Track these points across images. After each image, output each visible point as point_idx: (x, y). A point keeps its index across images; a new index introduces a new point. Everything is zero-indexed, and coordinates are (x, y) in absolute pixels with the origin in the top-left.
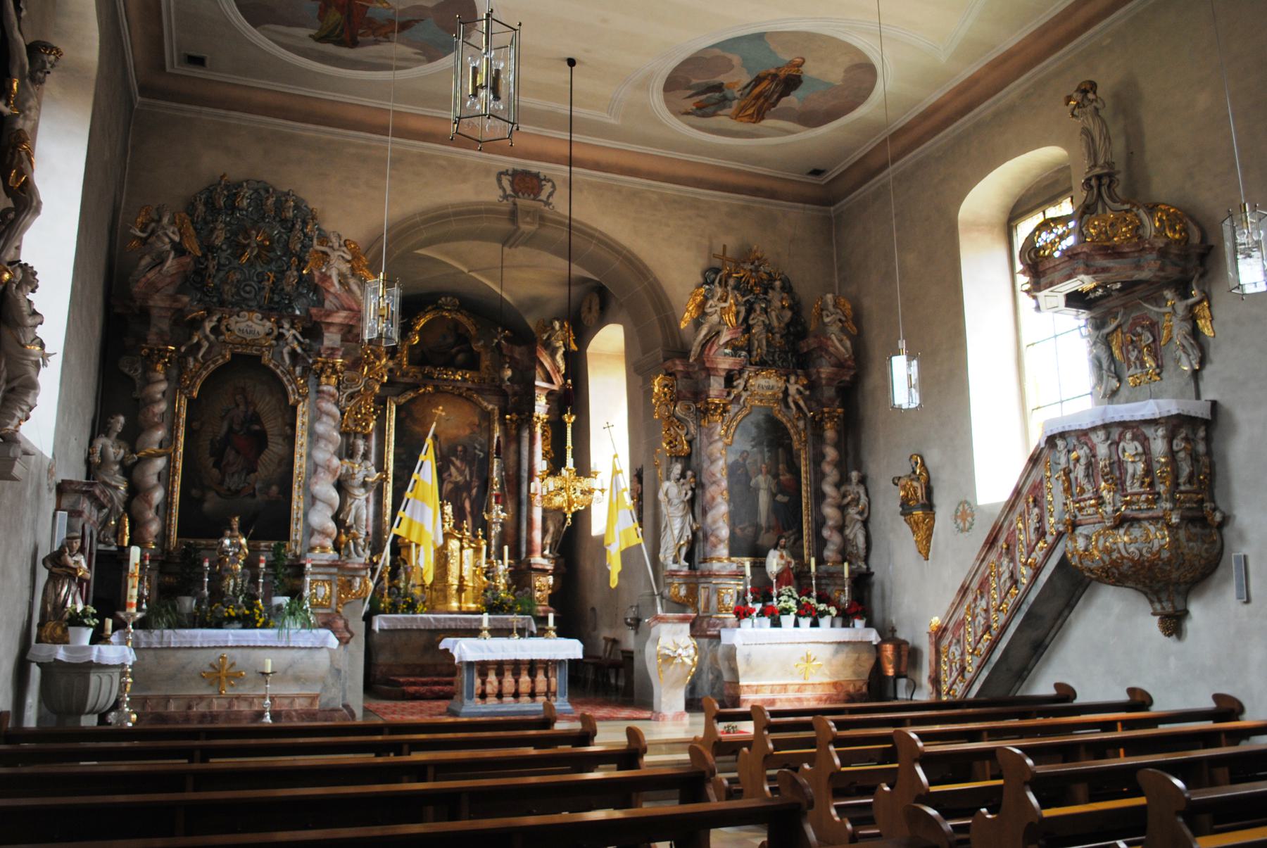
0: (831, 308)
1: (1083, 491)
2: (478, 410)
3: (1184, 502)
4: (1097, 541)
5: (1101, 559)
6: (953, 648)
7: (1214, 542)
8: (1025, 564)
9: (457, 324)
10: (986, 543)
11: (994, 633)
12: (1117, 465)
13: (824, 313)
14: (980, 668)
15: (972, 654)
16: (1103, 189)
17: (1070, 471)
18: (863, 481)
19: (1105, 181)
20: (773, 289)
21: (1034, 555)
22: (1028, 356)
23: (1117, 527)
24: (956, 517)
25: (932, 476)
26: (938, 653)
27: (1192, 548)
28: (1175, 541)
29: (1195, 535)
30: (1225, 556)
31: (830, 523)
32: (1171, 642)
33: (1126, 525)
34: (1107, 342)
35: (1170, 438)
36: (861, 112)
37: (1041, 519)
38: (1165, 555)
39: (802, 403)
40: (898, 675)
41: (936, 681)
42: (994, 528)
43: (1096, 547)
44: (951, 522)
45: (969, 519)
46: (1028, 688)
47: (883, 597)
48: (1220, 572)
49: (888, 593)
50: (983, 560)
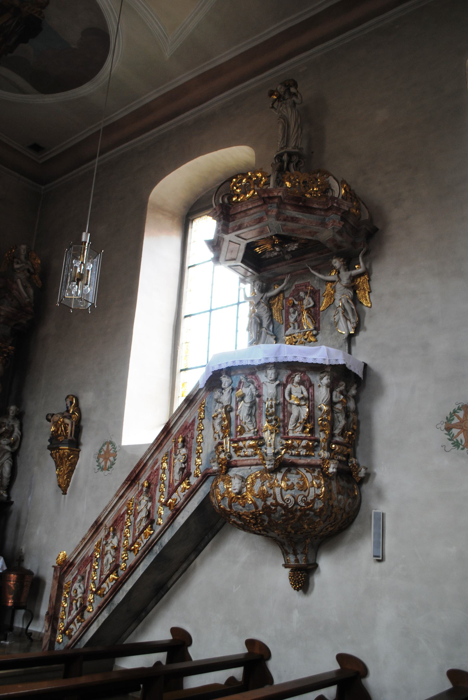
0: (23, 257)
3: (337, 453)
4: (253, 483)
5: (254, 504)
6: (76, 585)
7: (355, 497)
8: (164, 505)
10: (127, 480)
11: (121, 573)
12: (282, 406)
13: (15, 260)
14: (101, 609)
15: (95, 593)
16: (292, 166)
18: (20, 416)
19: (295, 158)
21: (175, 496)
22: (185, 324)
23: (274, 471)
25: (84, 416)
26: (60, 588)
27: (339, 502)
28: (329, 491)
29: (343, 487)
30: (361, 513)
32: (297, 597)
33: (284, 470)
34: (269, 303)
35: (331, 387)
37: (187, 460)
38: (319, 505)
40: (17, 606)
41: (53, 618)
42: (138, 465)
44: (93, 462)
45: (112, 459)
46: (144, 630)
47: (18, 526)
48: (355, 528)
49: (22, 523)
50: (121, 497)
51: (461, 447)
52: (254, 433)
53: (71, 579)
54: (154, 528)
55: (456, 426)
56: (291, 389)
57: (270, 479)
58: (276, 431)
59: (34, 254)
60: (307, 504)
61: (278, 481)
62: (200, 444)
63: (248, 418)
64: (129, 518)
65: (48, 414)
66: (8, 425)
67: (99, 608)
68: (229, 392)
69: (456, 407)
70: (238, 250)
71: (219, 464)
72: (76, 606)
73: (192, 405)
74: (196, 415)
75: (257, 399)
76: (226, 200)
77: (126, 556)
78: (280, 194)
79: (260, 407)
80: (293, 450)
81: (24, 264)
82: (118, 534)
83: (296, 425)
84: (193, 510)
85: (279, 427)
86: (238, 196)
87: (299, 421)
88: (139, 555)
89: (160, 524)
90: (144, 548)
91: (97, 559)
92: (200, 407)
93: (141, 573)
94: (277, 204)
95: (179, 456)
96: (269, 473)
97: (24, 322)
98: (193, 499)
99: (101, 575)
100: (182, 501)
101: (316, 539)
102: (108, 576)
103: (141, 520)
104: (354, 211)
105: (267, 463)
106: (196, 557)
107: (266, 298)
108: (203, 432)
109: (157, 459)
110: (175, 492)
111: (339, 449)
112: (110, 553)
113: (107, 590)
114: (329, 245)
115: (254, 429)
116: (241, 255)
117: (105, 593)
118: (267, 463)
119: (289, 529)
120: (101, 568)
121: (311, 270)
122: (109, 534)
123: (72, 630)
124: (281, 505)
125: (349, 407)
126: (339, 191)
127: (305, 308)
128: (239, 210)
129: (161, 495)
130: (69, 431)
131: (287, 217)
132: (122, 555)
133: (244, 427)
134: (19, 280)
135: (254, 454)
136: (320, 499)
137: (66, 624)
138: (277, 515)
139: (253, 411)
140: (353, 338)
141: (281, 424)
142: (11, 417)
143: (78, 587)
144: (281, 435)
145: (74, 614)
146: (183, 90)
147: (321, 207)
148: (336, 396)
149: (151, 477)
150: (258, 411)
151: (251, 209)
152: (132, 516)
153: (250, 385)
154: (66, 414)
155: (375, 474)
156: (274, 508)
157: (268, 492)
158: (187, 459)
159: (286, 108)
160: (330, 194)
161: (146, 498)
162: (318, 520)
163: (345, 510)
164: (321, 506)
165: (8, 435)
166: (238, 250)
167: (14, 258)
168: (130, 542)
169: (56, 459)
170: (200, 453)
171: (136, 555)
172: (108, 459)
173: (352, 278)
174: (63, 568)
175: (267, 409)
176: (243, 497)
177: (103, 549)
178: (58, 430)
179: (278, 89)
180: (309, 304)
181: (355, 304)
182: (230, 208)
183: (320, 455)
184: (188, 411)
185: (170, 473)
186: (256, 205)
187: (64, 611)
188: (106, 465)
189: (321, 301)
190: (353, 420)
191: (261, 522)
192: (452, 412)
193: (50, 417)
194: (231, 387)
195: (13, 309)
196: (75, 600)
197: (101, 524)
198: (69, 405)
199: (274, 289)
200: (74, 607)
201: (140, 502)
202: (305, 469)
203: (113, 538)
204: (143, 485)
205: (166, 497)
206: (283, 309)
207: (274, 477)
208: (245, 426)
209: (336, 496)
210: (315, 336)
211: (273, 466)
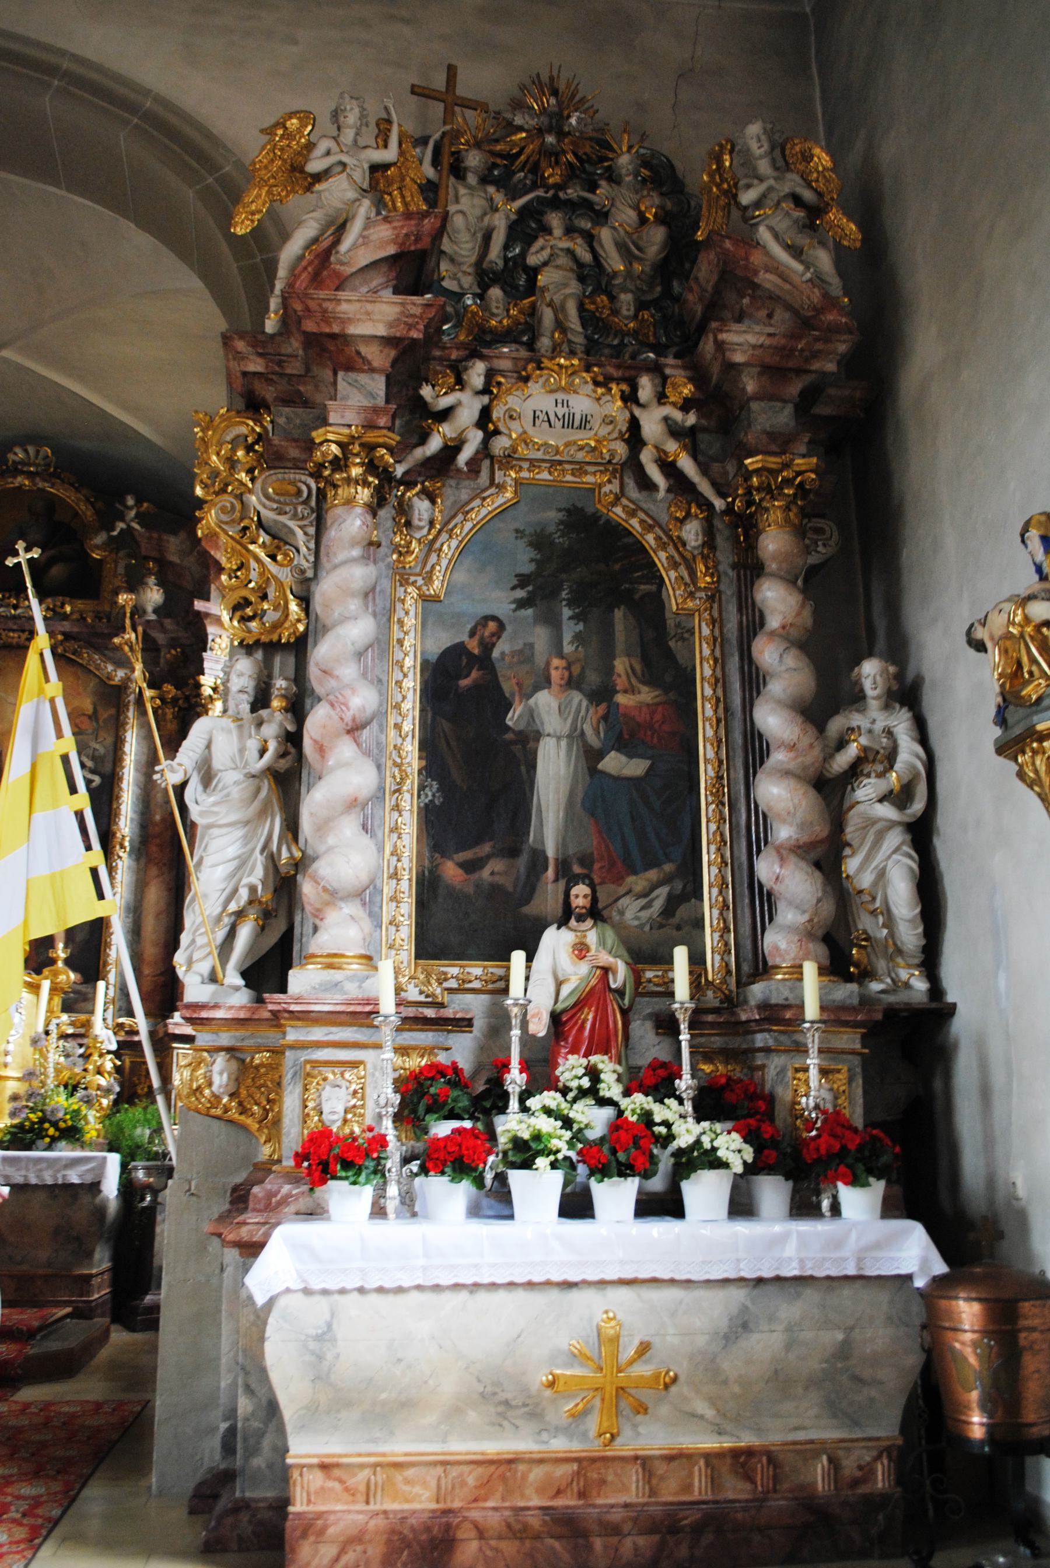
0: (764, 166)
2: (93, 683)
9: (52, 503)
18: (907, 694)
20: (613, 179)
31: (784, 833)
39: (686, 464)
47: (986, 1094)
49: (998, 1079)
66: (870, 731)
97: (831, 367)
165: (880, 768)
169: (1041, 786)
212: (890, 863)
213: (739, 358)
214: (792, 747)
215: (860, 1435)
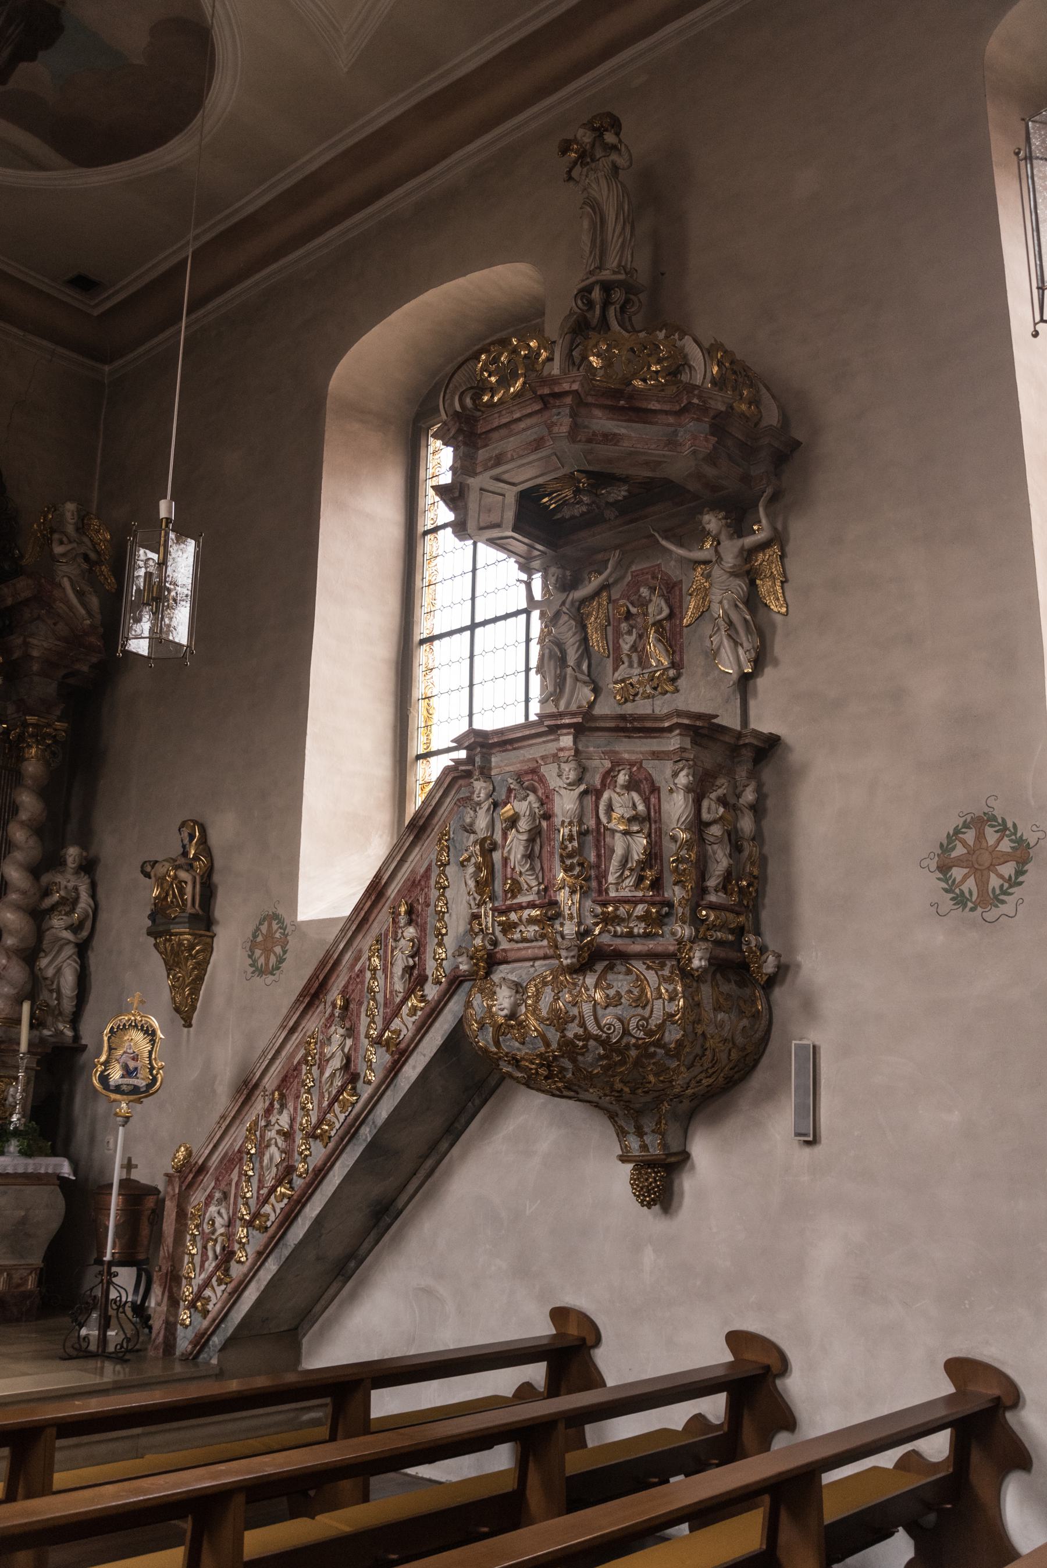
0: (70, 529)
1: (516, 889)
3: (713, 927)
5: (542, 1036)
6: (213, 1209)
7: (756, 1016)
8: (377, 1042)
10: (302, 995)
11: (298, 1182)
12: (592, 835)
13: (56, 536)
14: (262, 1256)
15: (249, 1224)
16: (611, 312)
17: (494, 847)
18: (88, 867)
19: (618, 295)
21: (396, 1024)
23: (581, 968)
24: (253, 945)
25: (218, 864)
27: (721, 1025)
28: (694, 1005)
30: (773, 1046)
32: (650, 1220)
33: (600, 967)
36: (176, 151)
37: (417, 951)
38: (673, 1035)
42: (323, 963)
43: (535, 1011)
45: (278, 950)
48: (759, 1078)
50: (293, 1030)
51: (970, 905)
52: (538, 892)
53: (203, 1199)
54: (358, 1091)
55: (959, 862)
56: (610, 799)
57: (572, 987)
58: (581, 888)
59: (96, 522)
60: (650, 1033)
61: (587, 989)
62: (443, 917)
63: (526, 863)
64: (310, 1072)
65: (145, 862)
67: (259, 1254)
68: (488, 809)
69: (960, 822)
70: (503, 507)
71: (472, 958)
72: (215, 1252)
73: (425, 837)
74: (434, 857)
75: (544, 824)
76: (468, 402)
77: (306, 1149)
78: (575, 387)
79: (550, 840)
80: (618, 925)
81: (75, 545)
82: (291, 1105)
83: (622, 874)
84: (435, 1051)
85: (587, 879)
86: (493, 391)
87: (629, 865)
88: (331, 1145)
89: (369, 1082)
90: (340, 1132)
91: (251, 1158)
92: (440, 840)
93: (338, 1182)
94: (572, 408)
95: (402, 942)
96: (570, 974)
97: (85, 669)
98: (433, 1030)
99: (259, 1188)
100: (410, 1034)
101: (681, 1102)
102: (273, 1190)
103: (333, 1075)
104: (744, 407)
105: (564, 953)
106: (452, 1145)
107: (573, 602)
108: (448, 893)
109: (360, 951)
110: (396, 1016)
111: (717, 918)
112: (276, 1144)
113: (272, 1218)
114: (693, 486)
115: (540, 884)
116: (510, 515)
117: (269, 1224)
118: (564, 953)
119: (618, 1086)
120: (260, 1175)
121: (660, 539)
122: (272, 1104)
123: (209, 1299)
124: (597, 1038)
125: (742, 829)
126: (702, 370)
127: (651, 621)
128: (496, 424)
129: (370, 1022)
130: (188, 896)
131: (594, 434)
132: (299, 1147)
133: (518, 883)
134: (65, 579)
135: (541, 936)
136: (674, 1023)
137: (196, 1289)
138: (589, 1058)
139: (537, 848)
140: (751, 682)
141: (593, 873)
142: (71, 871)
143: (216, 1215)
144: (594, 895)
145: (211, 1269)
146: (384, 140)
147: (666, 407)
148: (709, 809)
149: (350, 988)
150: (547, 848)
151: (519, 420)
152: (315, 1068)
153: (528, 795)
154: (182, 861)
155: (798, 966)
156: (581, 1044)
157: (567, 1012)
158: (418, 949)
159: (597, 180)
160: (685, 377)
161: (341, 1031)
162: (674, 1064)
163: (734, 1043)
164: (678, 1037)
165: (67, 909)
166: (503, 507)
167: (53, 531)
168: (314, 1120)
170: (443, 935)
171: (325, 1147)
172: (271, 950)
173: (745, 554)
174: (186, 1178)
175: (563, 843)
176: (520, 1024)
177: (262, 1136)
178: (167, 895)
179: (579, 136)
180: (661, 612)
181: (753, 611)
182: (476, 420)
183: (673, 934)
184: (417, 849)
185: (386, 978)
186: (529, 411)
187: (192, 1263)
188: (267, 964)
189: (684, 606)
190: (750, 856)
191: (560, 1072)
192: (951, 833)
193: (148, 869)
194: (491, 800)
195: (58, 643)
196: (212, 1239)
197: (256, 1086)
198: (186, 841)
199: (590, 582)
200: (210, 1254)
201: (329, 1039)
202: (644, 964)
203: (280, 1112)
204: (334, 1005)
205: (380, 1026)
206: (609, 624)
207: (580, 982)
208: (521, 880)
209: (712, 1016)
210: (673, 680)
211: (575, 960)
212: (65, 964)
213: (35, 653)
214: (24, 893)
215: (23, 1262)
